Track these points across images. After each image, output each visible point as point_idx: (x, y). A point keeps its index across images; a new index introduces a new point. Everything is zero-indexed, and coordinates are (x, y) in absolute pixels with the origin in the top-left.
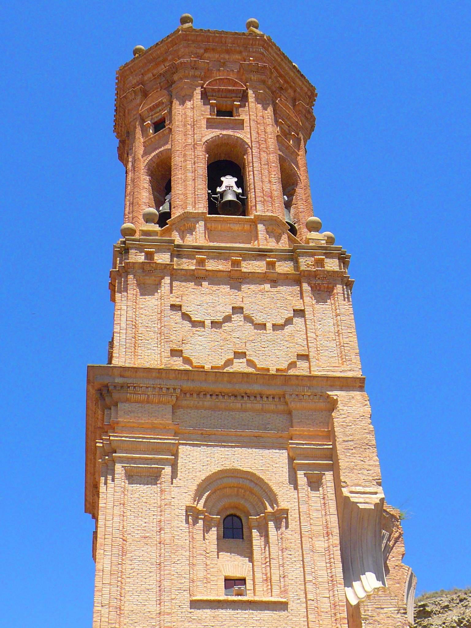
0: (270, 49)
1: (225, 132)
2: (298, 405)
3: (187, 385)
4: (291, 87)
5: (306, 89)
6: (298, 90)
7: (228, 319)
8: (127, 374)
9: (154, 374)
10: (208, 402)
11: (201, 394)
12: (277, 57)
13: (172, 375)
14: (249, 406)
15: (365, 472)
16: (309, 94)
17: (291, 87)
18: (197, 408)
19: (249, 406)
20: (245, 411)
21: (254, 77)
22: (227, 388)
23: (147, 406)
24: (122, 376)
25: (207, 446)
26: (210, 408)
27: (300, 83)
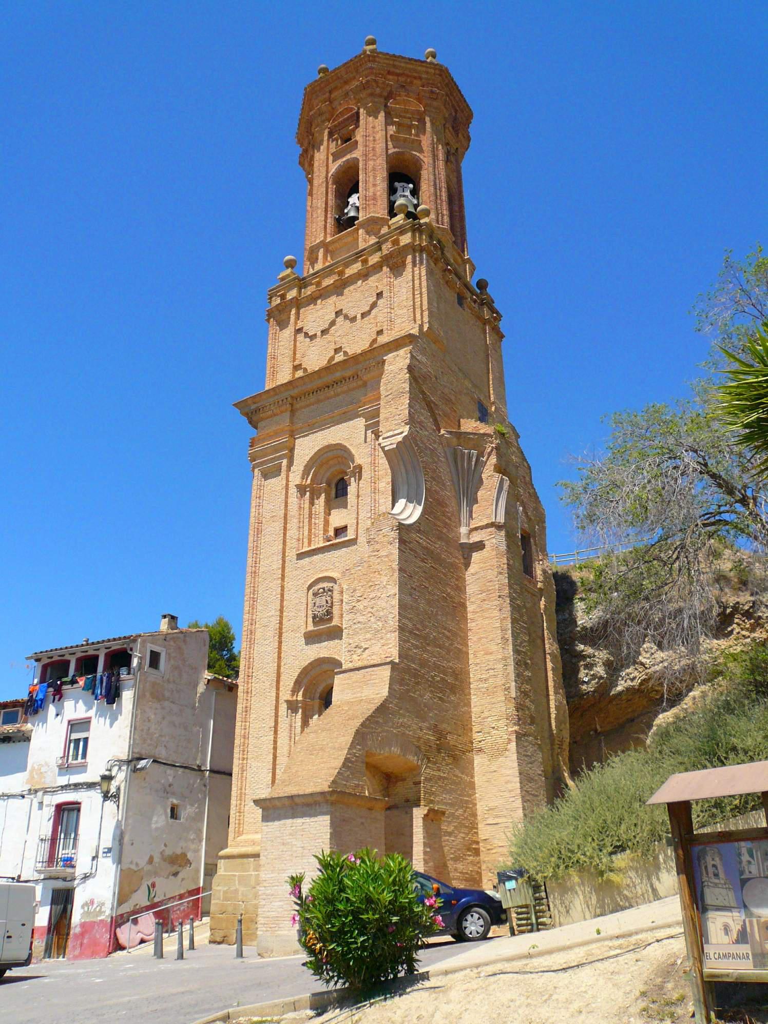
0: (377, 59)
1: (344, 159)
2: (369, 376)
3: (294, 392)
4: (415, 78)
5: (432, 71)
6: (424, 76)
7: (333, 323)
9: (272, 393)
10: (313, 399)
11: (307, 394)
14: (339, 390)
15: (397, 417)
16: (437, 72)
17: (415, 78)
18: (308, 406)
19: (339, 390)
20: (338, 395)
21: (363, 95)
22: (319, 383)
23: (275, 418)
27: (424, 69)
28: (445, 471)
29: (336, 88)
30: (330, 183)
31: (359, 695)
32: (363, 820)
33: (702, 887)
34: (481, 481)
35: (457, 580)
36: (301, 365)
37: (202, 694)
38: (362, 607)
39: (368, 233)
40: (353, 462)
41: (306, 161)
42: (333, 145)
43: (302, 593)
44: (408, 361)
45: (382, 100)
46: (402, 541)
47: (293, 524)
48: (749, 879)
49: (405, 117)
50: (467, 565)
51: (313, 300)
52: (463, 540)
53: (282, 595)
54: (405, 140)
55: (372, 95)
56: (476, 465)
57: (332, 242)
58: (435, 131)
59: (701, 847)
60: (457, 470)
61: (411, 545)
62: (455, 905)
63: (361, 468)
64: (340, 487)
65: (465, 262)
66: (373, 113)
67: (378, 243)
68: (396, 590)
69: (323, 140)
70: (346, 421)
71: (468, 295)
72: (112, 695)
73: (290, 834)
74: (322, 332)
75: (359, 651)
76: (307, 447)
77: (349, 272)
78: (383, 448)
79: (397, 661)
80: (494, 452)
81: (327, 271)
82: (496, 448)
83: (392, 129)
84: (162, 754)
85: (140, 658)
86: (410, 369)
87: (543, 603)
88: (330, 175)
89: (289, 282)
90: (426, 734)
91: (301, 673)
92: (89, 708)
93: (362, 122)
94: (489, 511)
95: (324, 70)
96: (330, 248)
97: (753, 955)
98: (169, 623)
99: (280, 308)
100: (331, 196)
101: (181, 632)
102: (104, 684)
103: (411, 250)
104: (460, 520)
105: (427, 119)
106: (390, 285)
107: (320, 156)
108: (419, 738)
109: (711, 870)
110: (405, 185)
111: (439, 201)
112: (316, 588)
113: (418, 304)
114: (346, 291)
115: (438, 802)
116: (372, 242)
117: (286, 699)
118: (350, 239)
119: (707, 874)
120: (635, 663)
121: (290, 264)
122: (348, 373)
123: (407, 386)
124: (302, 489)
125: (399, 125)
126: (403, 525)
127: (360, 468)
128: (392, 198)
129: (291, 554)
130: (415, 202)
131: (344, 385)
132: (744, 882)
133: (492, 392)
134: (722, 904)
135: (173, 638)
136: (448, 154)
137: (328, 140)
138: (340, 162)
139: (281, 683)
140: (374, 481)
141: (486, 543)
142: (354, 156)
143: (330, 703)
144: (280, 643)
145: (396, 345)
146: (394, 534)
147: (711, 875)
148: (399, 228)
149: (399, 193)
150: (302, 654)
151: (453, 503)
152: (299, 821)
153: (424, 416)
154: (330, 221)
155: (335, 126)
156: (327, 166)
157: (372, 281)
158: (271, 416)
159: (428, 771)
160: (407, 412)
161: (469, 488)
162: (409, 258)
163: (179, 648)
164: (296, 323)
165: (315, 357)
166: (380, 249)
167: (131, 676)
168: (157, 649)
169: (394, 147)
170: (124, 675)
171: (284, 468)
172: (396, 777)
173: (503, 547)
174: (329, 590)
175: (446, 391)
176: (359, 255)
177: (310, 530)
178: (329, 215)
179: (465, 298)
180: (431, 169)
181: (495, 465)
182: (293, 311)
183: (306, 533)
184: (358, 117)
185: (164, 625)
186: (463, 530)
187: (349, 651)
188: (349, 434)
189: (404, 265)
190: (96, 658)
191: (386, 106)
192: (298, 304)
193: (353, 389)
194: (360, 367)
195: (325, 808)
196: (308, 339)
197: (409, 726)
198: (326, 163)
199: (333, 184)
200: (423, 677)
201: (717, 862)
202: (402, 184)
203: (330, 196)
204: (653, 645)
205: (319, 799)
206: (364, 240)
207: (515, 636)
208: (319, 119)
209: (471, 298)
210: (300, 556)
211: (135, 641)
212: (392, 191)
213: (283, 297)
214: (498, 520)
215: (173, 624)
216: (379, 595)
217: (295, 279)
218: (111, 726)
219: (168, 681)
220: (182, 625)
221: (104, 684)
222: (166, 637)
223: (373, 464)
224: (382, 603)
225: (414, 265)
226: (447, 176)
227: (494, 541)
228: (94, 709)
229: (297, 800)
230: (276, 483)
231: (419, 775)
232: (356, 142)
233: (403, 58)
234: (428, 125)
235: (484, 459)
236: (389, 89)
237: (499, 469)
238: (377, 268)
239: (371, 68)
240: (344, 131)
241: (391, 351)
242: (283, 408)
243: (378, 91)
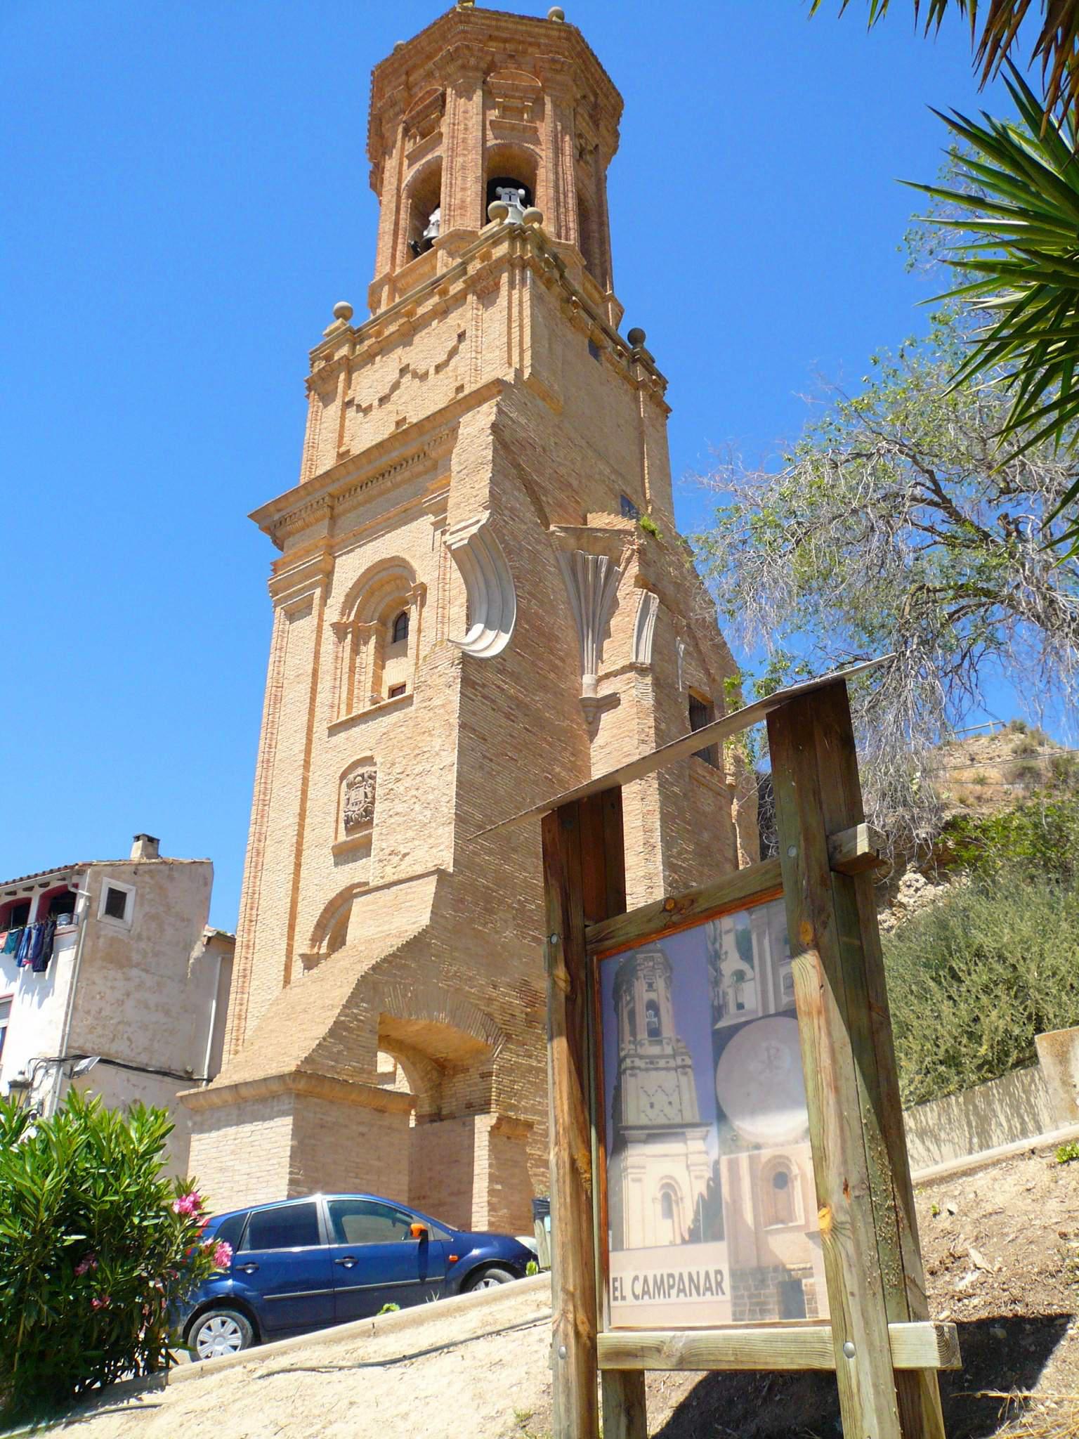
0: (473, 19)
1: (424, 161)
3: (333, 488)
4: (530, 44)
5: (555, 33)
7: (396, 386)
8: (282, 505)
9: (302, 493)
10: (361, 496)
11: (350, 490)
12: (487, 22)
13: (317, 485)
14: (399, 478)
17: (530, 44)
18: (355, 508)
21: (451, 69)
22: (367, 470)
23: (307, 531)
24: (279, 511)
25: (360, 546)
26: (366, 502)
27: (542, 31)
28: (556, 585)
29: (415, 67)
30: (404, 196)
31: (386, 928)
32: (363, 1129)
33: (620, 1074)
34: (615, 603)
35: (573, 755)
37: (197, 959)
38: (402, 788)
39: (451, 254)
40: (414, 580)
41: (376, 180)
42: (409, 147)
43: (332, 787)
44: (493, 418)
45: (479, 74)
46: (466, 681)
47: (325, 684)
48: (735, 1029)
49: (513, 97)
50: (593, 734)
51: (370, 358)
52: (587, 693)
53: (304, 792)
54: (513, 128)
55: (463, 67)
56: (607, 577)
58: (559, 115)
59: (621, 959)
60: (578, 592)
61: (485, 691)
62: (454, 1262)
63: (425, 590)
64: (401, 625)
65: (606, 300)
66: (465, 93)
67: (463, 263)
68: (454, 757)
69: (395, 142)
70: (406, 524)
71: (608, 343)
72: (42, 959)
73: (233, 1152)
75: (395, 859)
76: (350, 568)
77: (421, 311)
78: (449, 547)
79: (451, 870)
80: (635, 558)
81: (393, 314)
82: (639, 551)
83: (493, 114)
84: (120, 1049)
85: (89, 899)
86: (495, 428)
87: (735, 807)
88: (403, 186)
89: (338, 335)
90: (505, 995)
91: (326, 910)
92: (12, 978)
93: (449, 105)
94: (626, 648)
96: (399, 285)
97: (733, 1274)
98: (144, 848)
99: (324, 374)
100: (403, 215)
101: (164, 863)
102: (33, 941)
104: (583, 666)
105: (547, 100)
106: (477, 319)
107: (390, 164)
108: (491, 1000)
109: (644, 1018)
110: (513, 190)
111: (562, 210)
112: (351, 777)
113: (516, 340)
114: (417, 339)
115: (526, 1110)
116: (455, 263)
117: (301, 952)
118: (426, 268)
119: (633, 1033)
120: (891, 905)
121: (344, 314)
122: (410, 450)
123: (489, 454)
124: (340, 630)
125: (505, 109)
126: (472, 657)
127: (423, 588)
129: (321, 729)
131: (402, 470)
132: (722, 1039)
133: (647, 485)
134: (662, 1120)
135: (150, 871)
136: (580, 154)
138: (417, 166)
139: (297, 929)
140: (443, 606)
141: (622, 696)
142: (436, 154)
143: (343, 943)
144: (298, 866)
145: (467, 402)
146: (456, 672)
147: (643, 1035)
148: (492, 236)
150: (324, 880)
151: (571, 635)
152: (247, 1128)
153: (519, 500)
154: (401, 248)
155: (413, 118)
156: (400, 173)
157: (453, 319)
158: (303, 529)
159: (506, 1055)
160: (487, 490)
161: (595, 617)
162: (505, 277)
163: (161, 888)
164: (345, 394)
165: (367, 433)
166: (465, 272)
167: (72, 927)
168: (120, 886)
170: (63, 926)
171: (316, 601)
172: (454, 1067)
173: (649, 702)
174: (371, 777)
175: (562, 471)
176: (437, 286)
177: (351, 692)
178: (400, 240)
179: (599, 349)
180: (550, 166)
181: (636, 577)
182: (342, 376)
183: (344, 696)
184: (444, 105)
185: (136, 852)
186: (588, 679)
187: (380, 861)
188: (417, 545)
189: (497, 286)
190: (26, 903)
191: (484, 82)
192: (350, 367)
193: (419, 475)
194: (426, 438)
195: (287, 1103)
196: (361, 414)
197: (470, 979)
198: (401, 171)
199: (408, 198)
200: (501, 902)
201: (661, 993)
202: (507, 190)
203: (403, 215)
204: (918, 876)
205: (275, 1087)
206: (443, 262)
207: (668, 842)
208: (391, 113)
209: (614, 349)
210: (334, 730)
211: (81, 872)
213: (328, 358)
214: (641, 659)
215: (151, 850)
216: (428, 767)
218: (40, 1004)
219: (139, 937)
220: (166, 852)
221: (33, 941)
222: (137, 869)
223: (442, 580)
224: (432, 781)
225: (512, 285)
226: (578, 180)
227: (634, 691)
228: (19, 981)
229: (244, 1092)
230: (306, 625)
231: (490, 1061)
232: (441, 135)
233: (511, 15)
234: (548, 107)
235: (621, 570)
236: (489, 58)
237: (642, 582)
238: (460, 299)
239: (464, 32)
240: (424, 124)
241: (469, 409)
242: (320, 513)
243: (473, 61)
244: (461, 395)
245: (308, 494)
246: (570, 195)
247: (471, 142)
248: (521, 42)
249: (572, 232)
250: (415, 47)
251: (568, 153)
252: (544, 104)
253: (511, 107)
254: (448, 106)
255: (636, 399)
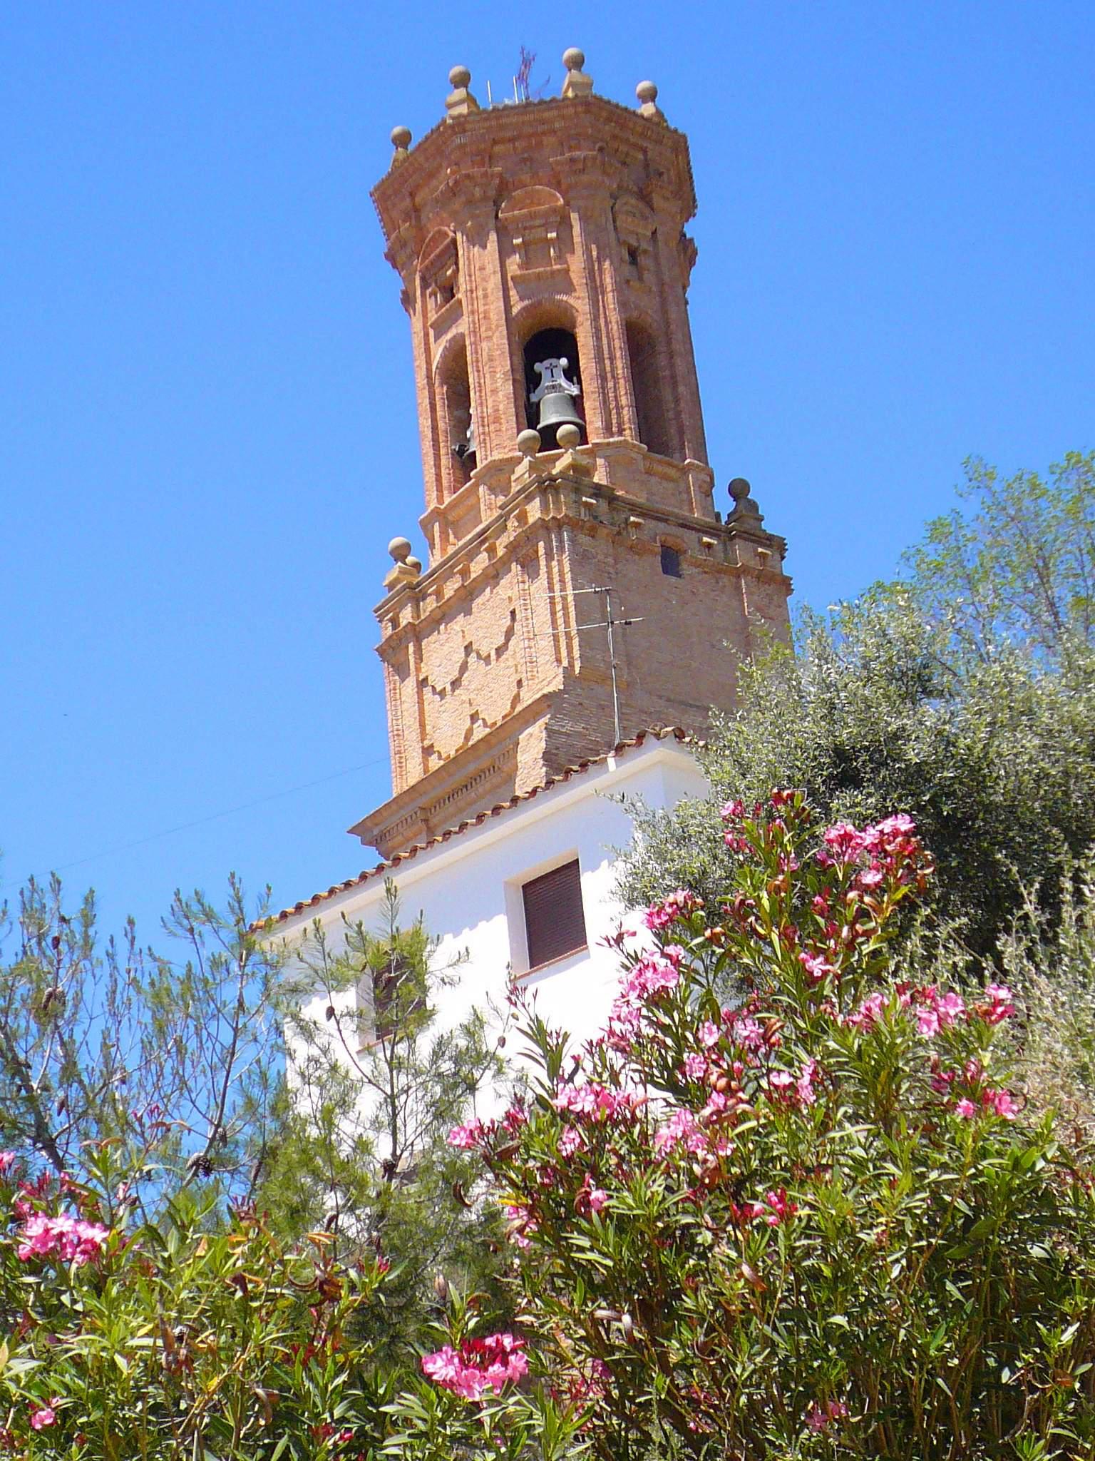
3: (423, 801)
4: (544, 133)
7: (464, 668)
17: (544, 133)
21: (457, 204)
27: (555, 113)
29: (418, 187)
36: (432, 746)
39: (492, 490)
57: (453, 506)
66: (478, 239)
67: (501, 516)
74: (453, 683)
95: (402, 140)
103: (541, 532)
105: (574, 217)
110: (554, 361)
121: (400, 553)
122: (485, 763)
128: (534, 398)
130: (575, 391)
137: (423, 295)
145: (519, 720)
149: (546, 382)
169: (522, 299)
178: (443, 451)
192: (418, 633)
202: (547, 363)
212: (531, 381)
217: (404, 588)
225: (549, 556)
232: (460, 302)
234: (577, 230)
242: (415, 828)
244: (519, 708)
245: (401, 808)
246: (618, 354)
247: (493, 316)
248: (530, 136)
249: (625, 412)
250: (411, 164)
251: (609, 288)
252: (571, 227)
253: (529, 242)
254: (460, 253)
255: (739, 588)
